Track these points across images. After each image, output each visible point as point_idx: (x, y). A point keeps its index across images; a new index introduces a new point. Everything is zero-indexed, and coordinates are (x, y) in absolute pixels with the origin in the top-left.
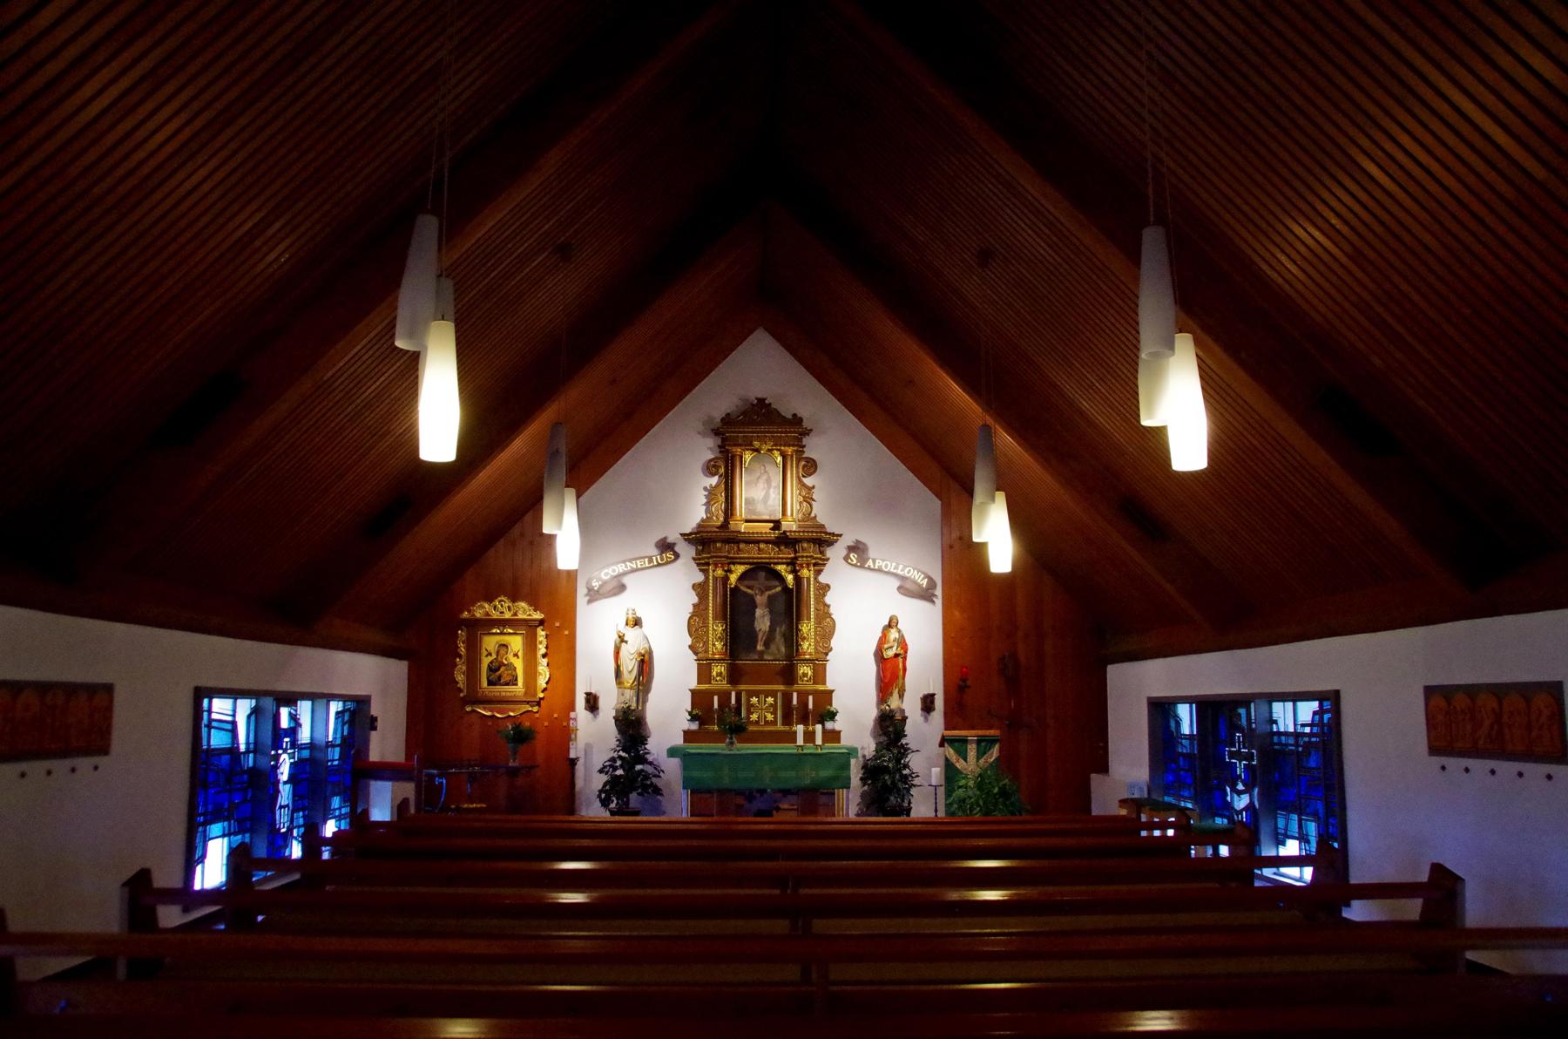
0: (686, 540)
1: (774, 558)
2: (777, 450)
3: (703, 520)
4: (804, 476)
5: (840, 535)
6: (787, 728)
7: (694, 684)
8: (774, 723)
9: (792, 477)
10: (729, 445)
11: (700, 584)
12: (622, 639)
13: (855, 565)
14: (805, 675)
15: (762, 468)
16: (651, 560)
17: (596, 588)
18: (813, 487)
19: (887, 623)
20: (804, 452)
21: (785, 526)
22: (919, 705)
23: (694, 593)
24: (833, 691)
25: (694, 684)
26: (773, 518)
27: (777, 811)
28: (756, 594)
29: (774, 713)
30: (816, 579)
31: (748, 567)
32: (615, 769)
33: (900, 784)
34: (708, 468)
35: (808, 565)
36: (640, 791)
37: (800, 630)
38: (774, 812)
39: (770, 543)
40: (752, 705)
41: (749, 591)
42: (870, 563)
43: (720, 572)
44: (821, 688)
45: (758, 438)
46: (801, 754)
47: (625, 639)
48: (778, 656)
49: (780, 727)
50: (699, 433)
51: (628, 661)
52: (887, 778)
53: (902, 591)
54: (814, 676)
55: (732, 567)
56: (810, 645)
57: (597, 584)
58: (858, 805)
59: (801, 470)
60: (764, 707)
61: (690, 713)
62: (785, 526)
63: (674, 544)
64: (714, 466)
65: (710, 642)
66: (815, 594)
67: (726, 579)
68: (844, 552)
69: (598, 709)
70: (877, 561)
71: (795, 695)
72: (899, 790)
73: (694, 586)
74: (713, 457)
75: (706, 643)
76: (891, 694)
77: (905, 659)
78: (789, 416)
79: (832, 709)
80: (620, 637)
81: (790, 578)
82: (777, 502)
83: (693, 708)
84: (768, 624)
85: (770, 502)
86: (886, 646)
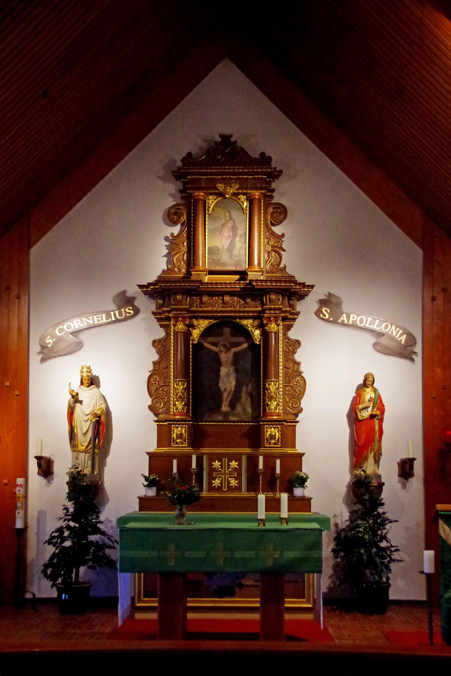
0: (145, 293)
1: (240, 312)
2: (243, 194)
3: (164, 272)
4: (273, 225)
5: (312, 287)
6: (252, 494)
7: (153, 447)
8: (238, 489)
9: (260, 224)
10: (191, 189)
11: (160, 341)
12: (76, 399)
13: (327, 321)
14: (272, 437)
15: (227, 214)
16: (108, 315)
17: (49, 346)
18: (283, 235)
19: (362, 382)
20: (272, 197)
21: (251, 276)
22: (395, 470)
23: (154, 350)
24: (303, 454)
25: (153, 447)
26: (238, 269)
27: (240, 588)
28: (221, 351)
29: (239, 478)
30: (285, 334)
31: (212, 321)
32: (64, 539)
33: (378, 560)
34: (169, 215)
35: (276, 319)
36: (91, 563)
37: (268, 389)
38: (237, 590)
39: (235, 295)
40: (236, 479)
41: (213, 348)
42: (344, 318)
43: (181, 326)
44: (290, 451)
45: (223, 181)
46: (262, 531)
47: (80, 399)
48: (244, 418)
49: (244, 494)
50: (160, 178)
51: (83, 423)
52: (362, 551)
53: (378, 348)
54: (282, 438)
55: (195, 322)
56: (278, 405)
57: (51, 341)
58: (330, 577)
59: (269, 217)
60: (227, 472)
61: (146, 479)
62: (251, 276)
63: (134, 298)
64: (175, 214)
65: (172, 402)
66: (284, 351)
67: (187, 335)
68: (316, 307)
69: (52, 473)
70: (352, 316)
71: (261, 458)
72: (376, 565)
73: (154, 343)
74: (175, 203)
75: (167, 404)
76: (366, 459)
77: (381, 420)
78: (256, 155)
79: (301, 474)
80: (73, 396)
81: (257, 333)
82: (243, 252)
83: (150, 473)
84: (234, 383)
85: (236, 252)
86: (361, 407)
